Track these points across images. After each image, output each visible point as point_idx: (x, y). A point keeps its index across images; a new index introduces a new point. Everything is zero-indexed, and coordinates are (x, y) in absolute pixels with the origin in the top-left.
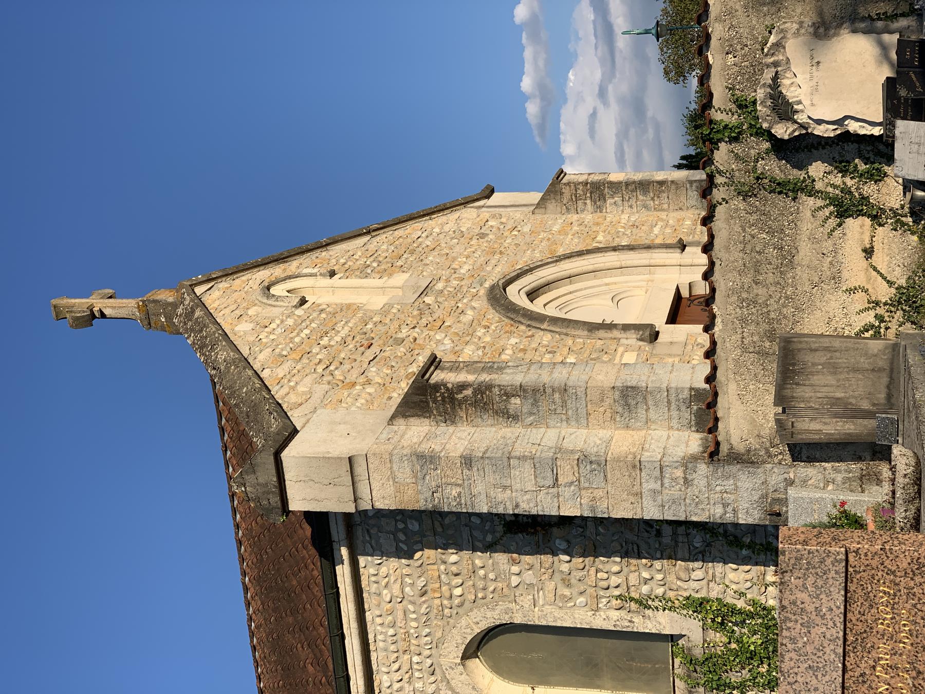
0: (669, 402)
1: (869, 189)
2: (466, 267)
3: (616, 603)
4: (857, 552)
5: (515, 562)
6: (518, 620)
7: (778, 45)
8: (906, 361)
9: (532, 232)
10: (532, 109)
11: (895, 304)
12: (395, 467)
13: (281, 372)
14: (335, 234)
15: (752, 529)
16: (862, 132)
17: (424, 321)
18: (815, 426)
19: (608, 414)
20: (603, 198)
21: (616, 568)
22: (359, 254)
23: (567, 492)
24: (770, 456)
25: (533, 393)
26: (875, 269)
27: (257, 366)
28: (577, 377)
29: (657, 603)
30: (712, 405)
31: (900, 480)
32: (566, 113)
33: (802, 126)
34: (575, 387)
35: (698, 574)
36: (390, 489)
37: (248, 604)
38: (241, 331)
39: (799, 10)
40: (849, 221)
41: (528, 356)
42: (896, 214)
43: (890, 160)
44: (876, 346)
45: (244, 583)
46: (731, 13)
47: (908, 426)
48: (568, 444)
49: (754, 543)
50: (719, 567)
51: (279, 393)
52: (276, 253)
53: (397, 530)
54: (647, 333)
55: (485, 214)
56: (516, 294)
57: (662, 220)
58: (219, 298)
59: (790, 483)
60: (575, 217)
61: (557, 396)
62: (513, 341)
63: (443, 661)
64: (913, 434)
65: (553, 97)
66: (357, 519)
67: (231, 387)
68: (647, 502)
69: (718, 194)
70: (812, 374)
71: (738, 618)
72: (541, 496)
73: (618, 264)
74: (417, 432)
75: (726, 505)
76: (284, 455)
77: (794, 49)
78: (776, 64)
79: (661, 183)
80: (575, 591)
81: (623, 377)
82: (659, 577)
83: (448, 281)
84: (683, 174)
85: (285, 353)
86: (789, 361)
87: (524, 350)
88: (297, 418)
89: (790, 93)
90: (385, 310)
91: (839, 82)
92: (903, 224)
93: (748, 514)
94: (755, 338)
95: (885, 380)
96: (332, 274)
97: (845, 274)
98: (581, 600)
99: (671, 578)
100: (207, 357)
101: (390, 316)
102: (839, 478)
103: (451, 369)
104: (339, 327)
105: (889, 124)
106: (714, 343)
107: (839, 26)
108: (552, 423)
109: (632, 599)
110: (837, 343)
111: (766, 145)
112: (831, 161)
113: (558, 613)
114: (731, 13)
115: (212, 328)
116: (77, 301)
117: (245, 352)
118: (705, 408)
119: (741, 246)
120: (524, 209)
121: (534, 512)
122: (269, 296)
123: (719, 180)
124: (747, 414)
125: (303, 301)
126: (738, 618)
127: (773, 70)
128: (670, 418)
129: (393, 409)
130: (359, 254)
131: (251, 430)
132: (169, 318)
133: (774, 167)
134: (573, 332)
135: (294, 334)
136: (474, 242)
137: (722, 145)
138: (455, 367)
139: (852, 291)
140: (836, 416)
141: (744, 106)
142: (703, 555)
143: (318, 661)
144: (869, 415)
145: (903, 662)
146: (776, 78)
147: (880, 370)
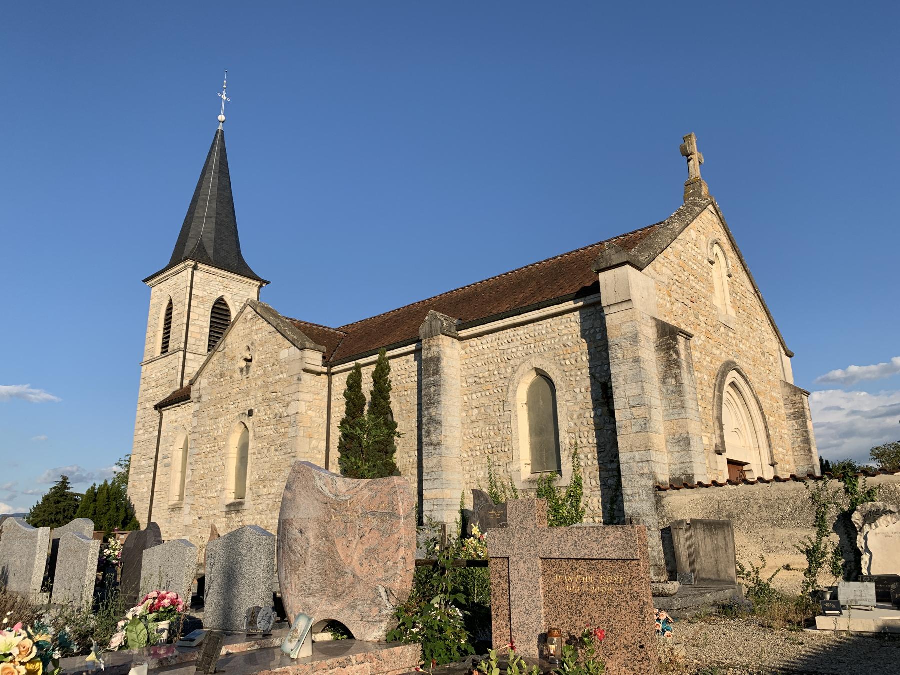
0: (684, 463)
1: (827, 568)
2: (744, 347)
3: (573, 442)
4: (639, 565)
5: (587, 390)
8: (727, 589)
9: (770, 381)
10: (838, 373)
11: (758, 582)
12: (629, 324)
13: (672, 257)
15: (622, 510)
16: (863, 563)
17: (710, 328)
18: (682, 541)
20: (796, 418)
21: (591, 441)
23: (628, 413)
25: (679, 390)
26: (778, 571)
28: (691, 413)
29: (576, 463)
30: (686, 486)
31: (661, 586)
32: (839, 393)
33: (861, 529)
35: (594, 483)
36: (617, 322)
37: (547, 261)
38: (691, 233)
40: (805, 557)
41: (698, 386)
42: (813, 583)
43: (848, 579)
44: (733, 573)
47: (689, 590)
48: (653, 411)
49: (614, 512)
50: (599, 493)
51: (660, 258)
52: (737, 244)
53: (595, 329)
55: (777, 354)
56: (732, 376)
58: (708, 220)
60: (782, 404)
61: (680, 403)
63: (533, 359)
64: (685, 593)
65: (848, 384)
66: (598, 308)
67: (659, 233)
68: (628, 455)
69: (811, 483)
70: (712, 538)
71: (574, 504)
73: (757, 429)
74: (650, 333)
75: (632, 495)
76: (628, 266)
79: (810, 451)
80: (576, 421)
82: (590, 463)
83: (735, 338)
84: (818, 463)
86: (718, 526)
87: (701, 384)
89: (882, 521)
90: (713, 307)
92: (808, 587)
93: (629, 508)
94: (727, 508)
95: (713, 577)
96: (730, 276)
97: (772, 555)
98: (573, 425)
99: (590, 469)
100: (674, 218)
102: (656, 554)
104: (700, 284)
105: (870, 579)
108: (664, 402)
110: (731, 551)
111: (846, 509)
113: (564, 413)
115: (691, 218)
117: (680, 237)
118: (684, 483)
121: (615, 397)
122: (712, 244)
123: (820, 483)
124: (683, 505)
126: (574, 504)
128: (675, 464)
131: (637, 247)
133: (832, 514)
134: (715, 409)
136: (759, 350)
137: (843, 484)
138: (688, 348)
140: (689, 552)
141: (870, 495)
142: (604, 485)
143: (526, 298)
144: (693, 569)
145: (585, 589)
146: (891, 512)
147: (719, 575)
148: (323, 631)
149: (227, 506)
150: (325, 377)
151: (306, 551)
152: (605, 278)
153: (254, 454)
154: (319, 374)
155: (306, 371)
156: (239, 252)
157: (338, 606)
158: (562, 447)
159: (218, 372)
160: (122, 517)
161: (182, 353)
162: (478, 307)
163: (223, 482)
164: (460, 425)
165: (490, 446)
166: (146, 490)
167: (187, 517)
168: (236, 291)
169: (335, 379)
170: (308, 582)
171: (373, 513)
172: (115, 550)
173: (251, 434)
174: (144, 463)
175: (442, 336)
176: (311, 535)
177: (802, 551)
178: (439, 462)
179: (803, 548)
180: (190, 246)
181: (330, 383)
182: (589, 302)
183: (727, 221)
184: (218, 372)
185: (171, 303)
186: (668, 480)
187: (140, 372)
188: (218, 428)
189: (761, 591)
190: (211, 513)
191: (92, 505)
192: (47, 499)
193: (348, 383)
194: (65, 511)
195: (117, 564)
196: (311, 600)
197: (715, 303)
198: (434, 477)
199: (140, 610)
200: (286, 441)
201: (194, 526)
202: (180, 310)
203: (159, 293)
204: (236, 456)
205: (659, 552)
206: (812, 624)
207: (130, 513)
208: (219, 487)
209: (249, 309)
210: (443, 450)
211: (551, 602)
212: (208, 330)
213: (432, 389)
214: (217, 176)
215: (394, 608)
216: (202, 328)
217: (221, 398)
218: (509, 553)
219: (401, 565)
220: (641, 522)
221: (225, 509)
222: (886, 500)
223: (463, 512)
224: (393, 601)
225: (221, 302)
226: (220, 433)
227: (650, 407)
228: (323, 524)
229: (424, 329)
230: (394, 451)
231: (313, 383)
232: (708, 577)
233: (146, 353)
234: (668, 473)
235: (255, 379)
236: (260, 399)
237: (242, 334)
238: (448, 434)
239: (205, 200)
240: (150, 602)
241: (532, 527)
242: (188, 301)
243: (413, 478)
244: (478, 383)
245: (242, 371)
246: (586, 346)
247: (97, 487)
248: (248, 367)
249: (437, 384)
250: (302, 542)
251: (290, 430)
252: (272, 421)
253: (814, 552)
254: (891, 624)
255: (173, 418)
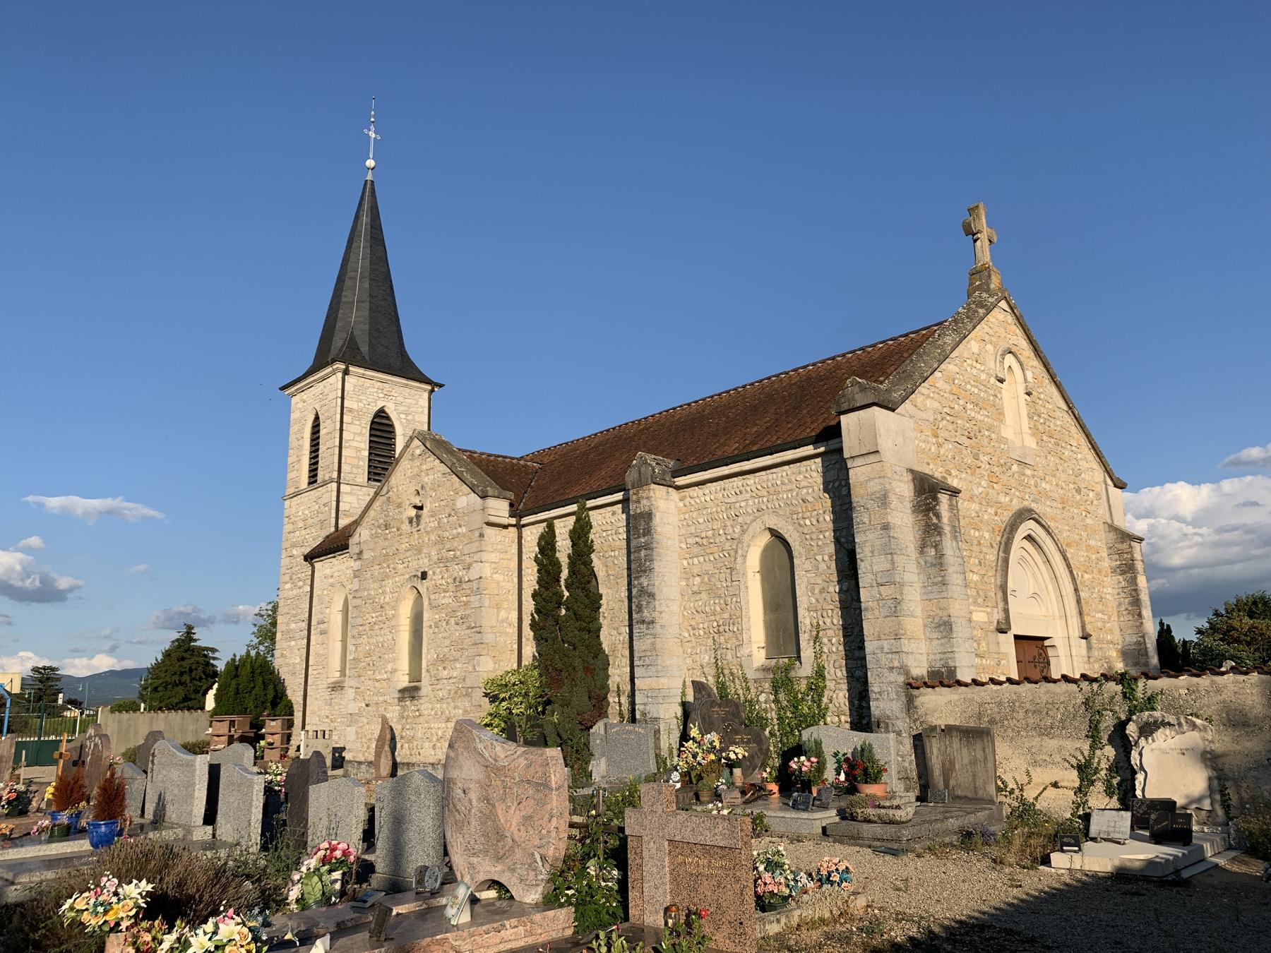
1: (1099, 786)
2: (1048, 487)
5: (830, 557)
6: (796, 561)
11: (1022, 801)
14: (1065, 386)
17: (996, 469)
18: (935, 751)
20: (1123, 573)
23: (875, 592)
24: (915, 721)
25: (940, 562)
27: (943, 366)
30: (942, 684)
31: (891, 812)
33: (1137, 742)
35: (839, 674)
36: (862, 478)
38: (972, 345)
40: (1076, 773)
42: (1084, 804)
44: (992, 789)
46: (1219, 691)
48: (907, 589)
50: (845, 687)
51: (923, 389)
52: (1042, 347)
56: (1028, 527)
59: (899, 733)
60: (1105, 554)
62: (987, 535)
67: (925, 352)
72: (870, 576)
73: (1064, 593)
74: (904, 489)
75: (880, 693)
76: (875, 408)
77: (1193, 738)
78: (1180, 724)
79: (1140, 615)
80: (818, 596)
83: (1033, 476)
87: (979, 543)
89: (1160, 734)
90: (1002, 440)
95: (969, 795)
96: (1029, 394)
97: (1038, 769)
98: (814, 600)
99: (834, 657)
102: (906, 764)
103: (951, 505)
106: (983, 684)
107: (1214, 769)
110: (990, 765)
112: (1116, 761)
113: (803, 586)
118: (943, 678)
123: (1095, 686)
124: (940, 707)
125: (1001, 381)
132: (978, 288)
133: (1108, 722)
136: (1072, 486)
137: (1120, 687)
138: (953, 507)
139: (1028, 773)
141: (1150, 702)
144: (947, 786)
147: (976, 792)
148: (488, 889)
150: (513, 530)
154: (506, 527)
156: (402, 345)
157: (499, 867)
158: (802, 628)
159: (381, 521)
161: (334, 485)
162: (704, 438)
163: (394, 660)
164: (678, 597)
166: (298, 659)
167: (349, 702)
169: (526, 531)
170: (472, 842)
171: (529, 782)
173: (426, 603)
174: (293, 626)
176: (473, 796)
178: (653, 644)
179: (1074, 762)
180: (338, 341)
181: (520, 537)
182: (832, 447)
183: (1027, 320)
184: (381, 521)
185: (317, 418)
186: (925, 673)
187: (283, 508)
188: (384, 593)
189: (1025, 812)
190: (381, 699)
191: (233, 682)
192: (167, 654)
193: (539, 544)
194: (191, 670)
196: (475, 860)
197: (1004, 434)
198: (648, 662)
199: (312, 862)
200: (468, 612)
201: (359, 715)
202: (330, 428)
203: (300, 405)
204: (408, 628)
205: (911, 762)
206: (1046, 861)
208: (389, 667)
209: (416, 442)
210: (658, 629)
211: (675, 880)
212: (367, 453)
213: (643, 553)
215: (549, 873)
216: (359, 450)
217: (386, 555)
218: (644, 833)
219: (553, 834)
221: (397, 695)
222: (1167, 709)
223: (684, 704)
224: (547, 866)
225: (381, 415)
226: (387, 599)
227: (902, 585)
228: (485, 786)
229: (631, 476)
231: (499, 538)
232: (963, 794)
233: (290, 483)
235: (428, 533)
236: (435, 558)
237: (409, 474)
238: (664, 608)
240: (321, 853)
241: (660, 811)
242: (338, 416)
244: (701, 545)
245: (411, 521)
248: (418, 517)
249: (648, 547)
251: (472, 599)
253: (1086, 767)
254: (1128, 864)
255: (328, 571)
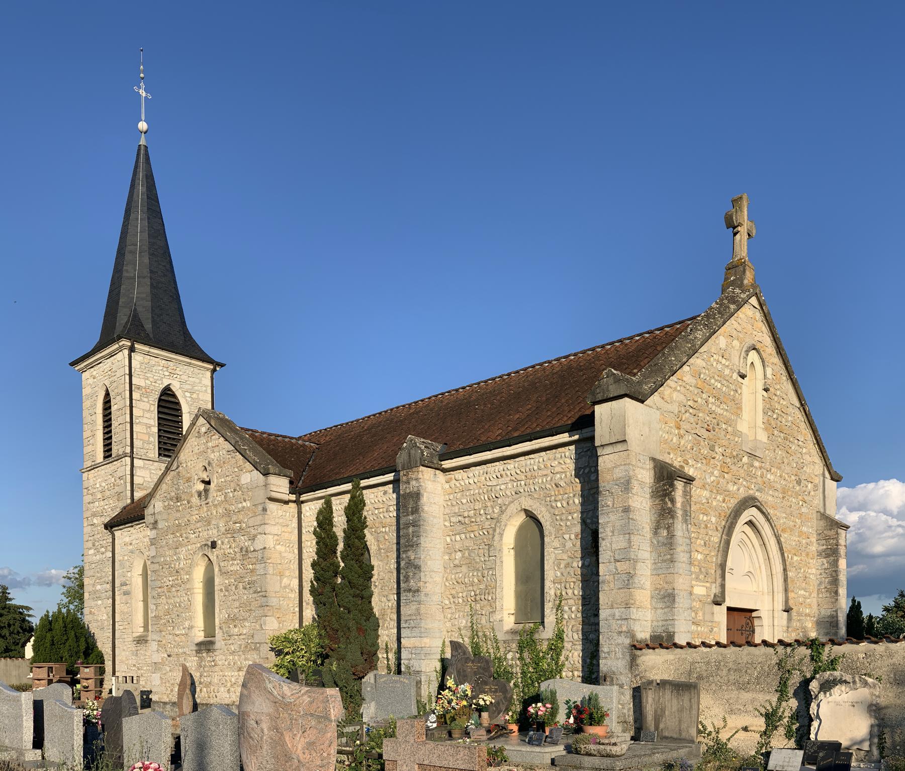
0: (666, 620)
1: (781, 731)
5: (576, 536)
6: (546, 539)
7: (866, 684)
11: (717, 741)
12: (622, 467)
18: (650, 700)
19: (659, 586)
20: (827, 556)
21: (576, 592)
22: (784, 403)
23: (612, 567)
25: (670, 543)
29: (559, 615)
30: (661, 646)
31: (608, 748)
33: (816, 696)
34: (674, 567)
35: (576, 637)
36: (609, 465)
39: (890, 695)
40: (763, 720)
42: (767, 744)
44: (694, 732)
45: (569, 355)
46: (891, 656)
48: (639, 565)
50: (580, 647)
53: (590, 467)
54: (718, 599)
56: (751, 513)
57: (810, 595)
58: (748, 321)
59: (621, 686)
61: (669, 557)
62: (713, 519)
63: (523, 498)
67: (676, 346)
69: (780, 649)
70: (678, 699)
71: (555, 657)
72: (610, 553)
73: (774, 572)
74: (645, 476)
76: (627, 399)
77: (863, 693)
78: (854, 682)
79: (836, 593)
80: (563, 570)
81: (682, 593)
82: (573, 616)
83: (761, 468)
85: (702, 376)
86: (684, 688)
87: (706, 527)
88: (655, 398)
89: (836, 690)
91: (841, 718)
92: (761, 748)
93: (605, 665)
95: (675, 736)
96: (766, 390)
97: (733, 717)
98: (559, 574)
99: (573, 622)
101: (732, 438)
102: (625, 711)
106: (695, 647)
107: (876, 718)
108: (653, 554)
109: (561, 601)
110: (694, 712)
113: (551, 561)
114: (891, 656)
116: (746, 213)
117: (701, 350)
118: (663, 641)
119: (750, 661)
120: (822, 505)
123: (789, 649)
124: (658, 665)
125: (743, 377)
126: (555, 657)
127: (851, 681)
128: (658, 621)
129: (661, 458)
130: (784, 403)
132: (733, 283)
133: (795, 680)
135: (717, 378)
136: (793, 477)
137: (809, 651)
138: (687, 494)
139: (725, 720)
141: (832, 664)
144: (657, 728)
149: (197, 644)
151: (262, 738)
152: (600, 411)
153: (221, 590)
155: (271, 499)
156: (183, 323)
158: (547, 597)
160: (83, 647)
161: (128, 459)
163: (191, 618)
165: (473, 593)
166: (104, 616)
168: (184, 377)
169: (305, 507)
172: (93, 710)
173: (216, 570)
174: (99, 587)
175: (422, 468)
176: (265, 726)
177: (761, 714)
178: (418, 610)
180: (123, 318)
181: (300, 513)
182: (585, 435)
185: (107, 394)
188: (179, 559)
190: (180, 650)
191: (49, 635)
193: (317, 519)
194: (9, 625)
195: (97, 723)
198: (412, 624)
200: (254, 578)
201: (163, 663)
203: (91, 381)
204: (201, 591)
205: (629, 709)
207: (90, 643)
208: (187, 624)
209: (201, 420)
212: (156, 430)
213: (411, 529)
214: (145, 216)
216: (149, 427)
217: (179, 525)
218: (398, 758)
220: (615, 679)
221: (195, 648)
222: (845, 670)
223: (443, 661)
227: (636, 561)
228: (274, 719)
230: (371, 596)
233: (86, 458)
234: (649, 630)
235: (215, 506)
236: (223, 529)
237: (196, 451)
239: (133, 253)
241: (412, 741)
242: (128, 393)
243: (392, 623)
244: (462, 523)
246: (579, 486)
247: (51, 614)
248: (206, 491)
249: (415, 524)
250: (258, 731)
251: (258, 567)
252: (238, 555)
255: (127, 539)
